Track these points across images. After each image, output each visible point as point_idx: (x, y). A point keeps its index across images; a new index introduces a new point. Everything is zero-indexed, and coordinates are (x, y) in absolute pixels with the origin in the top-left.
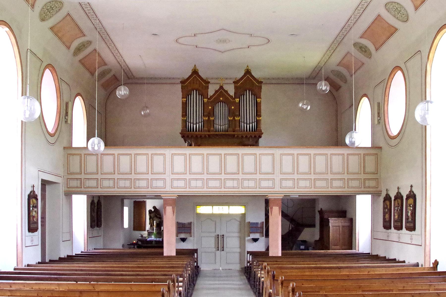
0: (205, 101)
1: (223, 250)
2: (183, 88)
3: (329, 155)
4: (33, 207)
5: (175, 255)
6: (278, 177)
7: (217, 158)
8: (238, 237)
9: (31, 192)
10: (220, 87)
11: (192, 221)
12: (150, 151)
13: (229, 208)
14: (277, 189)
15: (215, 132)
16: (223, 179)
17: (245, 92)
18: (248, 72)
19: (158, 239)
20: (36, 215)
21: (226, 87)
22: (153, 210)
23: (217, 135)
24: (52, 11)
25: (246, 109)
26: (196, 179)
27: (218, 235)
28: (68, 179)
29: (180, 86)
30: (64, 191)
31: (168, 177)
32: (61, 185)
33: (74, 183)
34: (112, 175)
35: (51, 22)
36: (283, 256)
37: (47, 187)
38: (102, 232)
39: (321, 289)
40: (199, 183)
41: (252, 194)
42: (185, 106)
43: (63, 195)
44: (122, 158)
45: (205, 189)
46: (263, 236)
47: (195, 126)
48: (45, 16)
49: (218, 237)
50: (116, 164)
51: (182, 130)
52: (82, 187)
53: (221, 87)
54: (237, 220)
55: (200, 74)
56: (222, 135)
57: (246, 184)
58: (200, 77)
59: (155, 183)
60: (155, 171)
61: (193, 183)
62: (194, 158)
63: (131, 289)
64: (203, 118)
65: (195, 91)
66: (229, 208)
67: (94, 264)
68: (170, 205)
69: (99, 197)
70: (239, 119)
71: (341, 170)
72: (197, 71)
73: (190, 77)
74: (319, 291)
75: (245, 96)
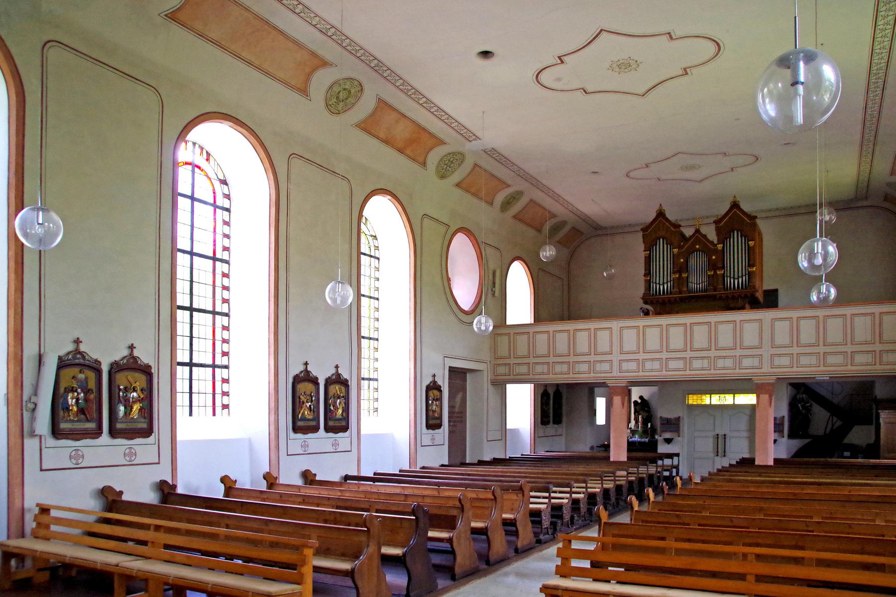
0: (750, 244)
1: (724, 456)
2: (644, 237)
3: (512, 334)
4: (434, 399)
5: (626, 460)
6: (766, 352)
7: (656, 331)
8: (746, 438)
9: (431, 382)
10: (695, 231)
11: (681, 415)
12: (592, 325)
13: (734, 397)
14: (766, 369)
15: (690, 293)
16: (664, 359)
17: (732, 234)
18: (735, 205)
19: (643, 440)
20: (438, 410)
21: (704, 230)
22: (639, 401)
23: (692, 297)
24: (452, 165)
25: (659, 265)
26: (653, 360)
27: (718, 435)
28: (495, 364)
29: (641, 234)
30: (491, 380)
31: (615, 357)
32: (485, 373)
33: (502, 370)
34: (815, 348)
35: (456, 177)
36: (630, 462)
37: (468, 375)
38: (564, 429)
39: (704, 508)
40: (656, 365)
41: (743, 378)
42: (648, 261)
43: (489, 384)
44: (558, 335)
45: (664, 373)
46: (783, 437)
47: (698, 286)
48: (445, 173)
49: (718, 438)
50: (551, 342)
51: (644, 294)
52: (512, 374)
53: (697, 231)
54: (746, 414)
55: (741, 207)
56: (697, 298)
57: (720, 363)
58: (667, 220)
59: (599, 367)
60: (578, 351)
61: (648, 365)
62: (649, 331)
63: (476, 496)
64: (748, 269)
65: (661, 240)
66: (734, 397)
67: (483, 468)
68: (618, 395)
69: (558, 385)
70: (723, 272)
71: (869, 338)
72: (737, 204)
73: (655, 220)
74: (875, 520)
75: (732, 240)
